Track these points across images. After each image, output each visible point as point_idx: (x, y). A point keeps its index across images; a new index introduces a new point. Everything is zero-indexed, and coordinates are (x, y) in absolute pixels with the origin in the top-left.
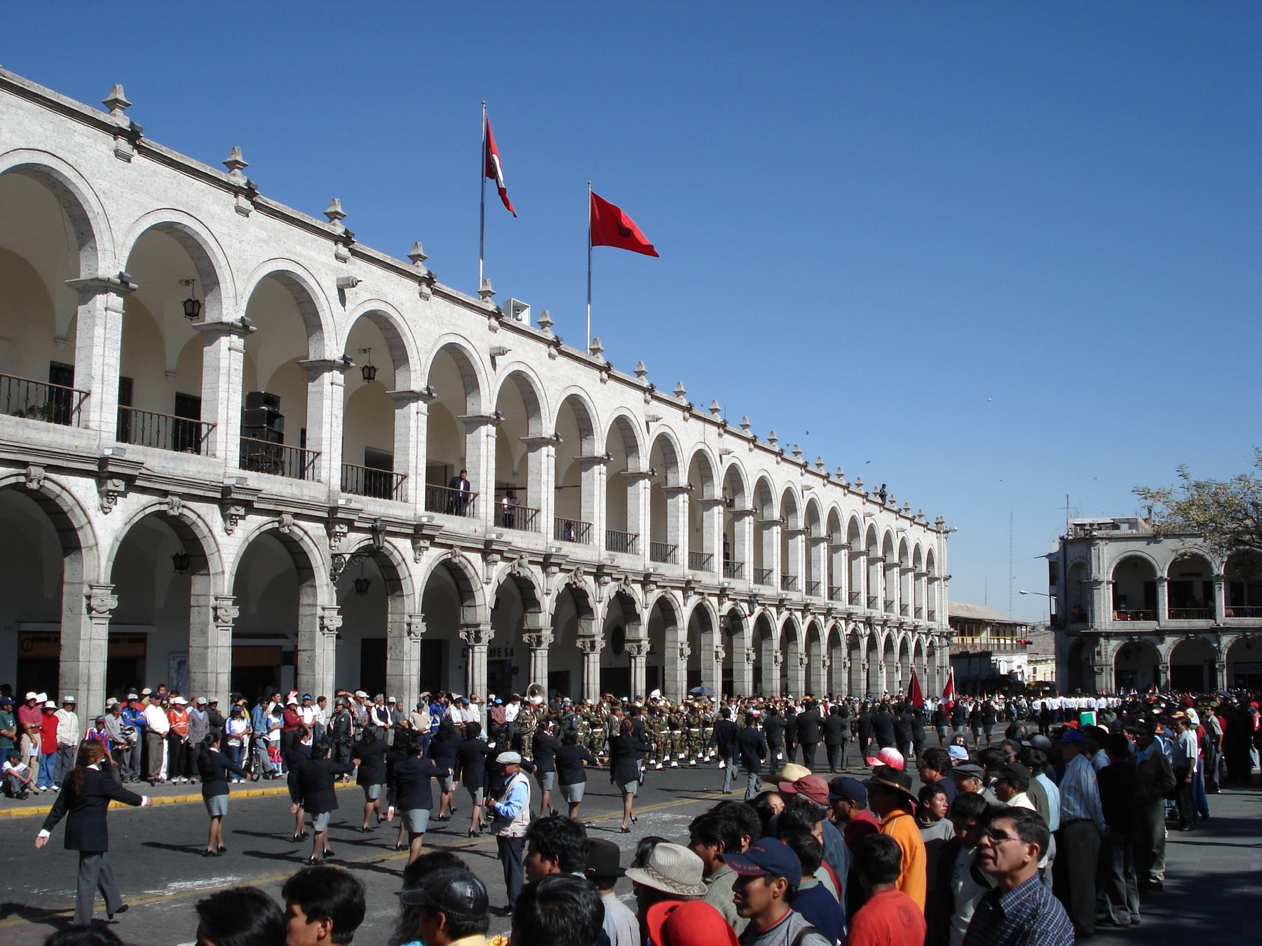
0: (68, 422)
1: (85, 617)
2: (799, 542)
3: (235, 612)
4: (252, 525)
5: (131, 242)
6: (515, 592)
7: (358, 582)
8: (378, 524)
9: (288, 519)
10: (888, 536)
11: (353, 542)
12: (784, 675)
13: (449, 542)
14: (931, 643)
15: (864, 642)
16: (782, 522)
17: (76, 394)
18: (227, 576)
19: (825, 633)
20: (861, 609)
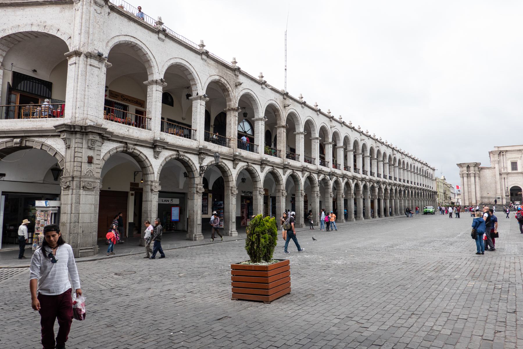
1: (150, 193)
5: (164, 71)
6: (271, 177)
9: (131, 146)
10: (399, 160)
11: (208, 161)
12: (355, 203)
13: (177, 149)
16: (383, 161)
19: (362, 187)
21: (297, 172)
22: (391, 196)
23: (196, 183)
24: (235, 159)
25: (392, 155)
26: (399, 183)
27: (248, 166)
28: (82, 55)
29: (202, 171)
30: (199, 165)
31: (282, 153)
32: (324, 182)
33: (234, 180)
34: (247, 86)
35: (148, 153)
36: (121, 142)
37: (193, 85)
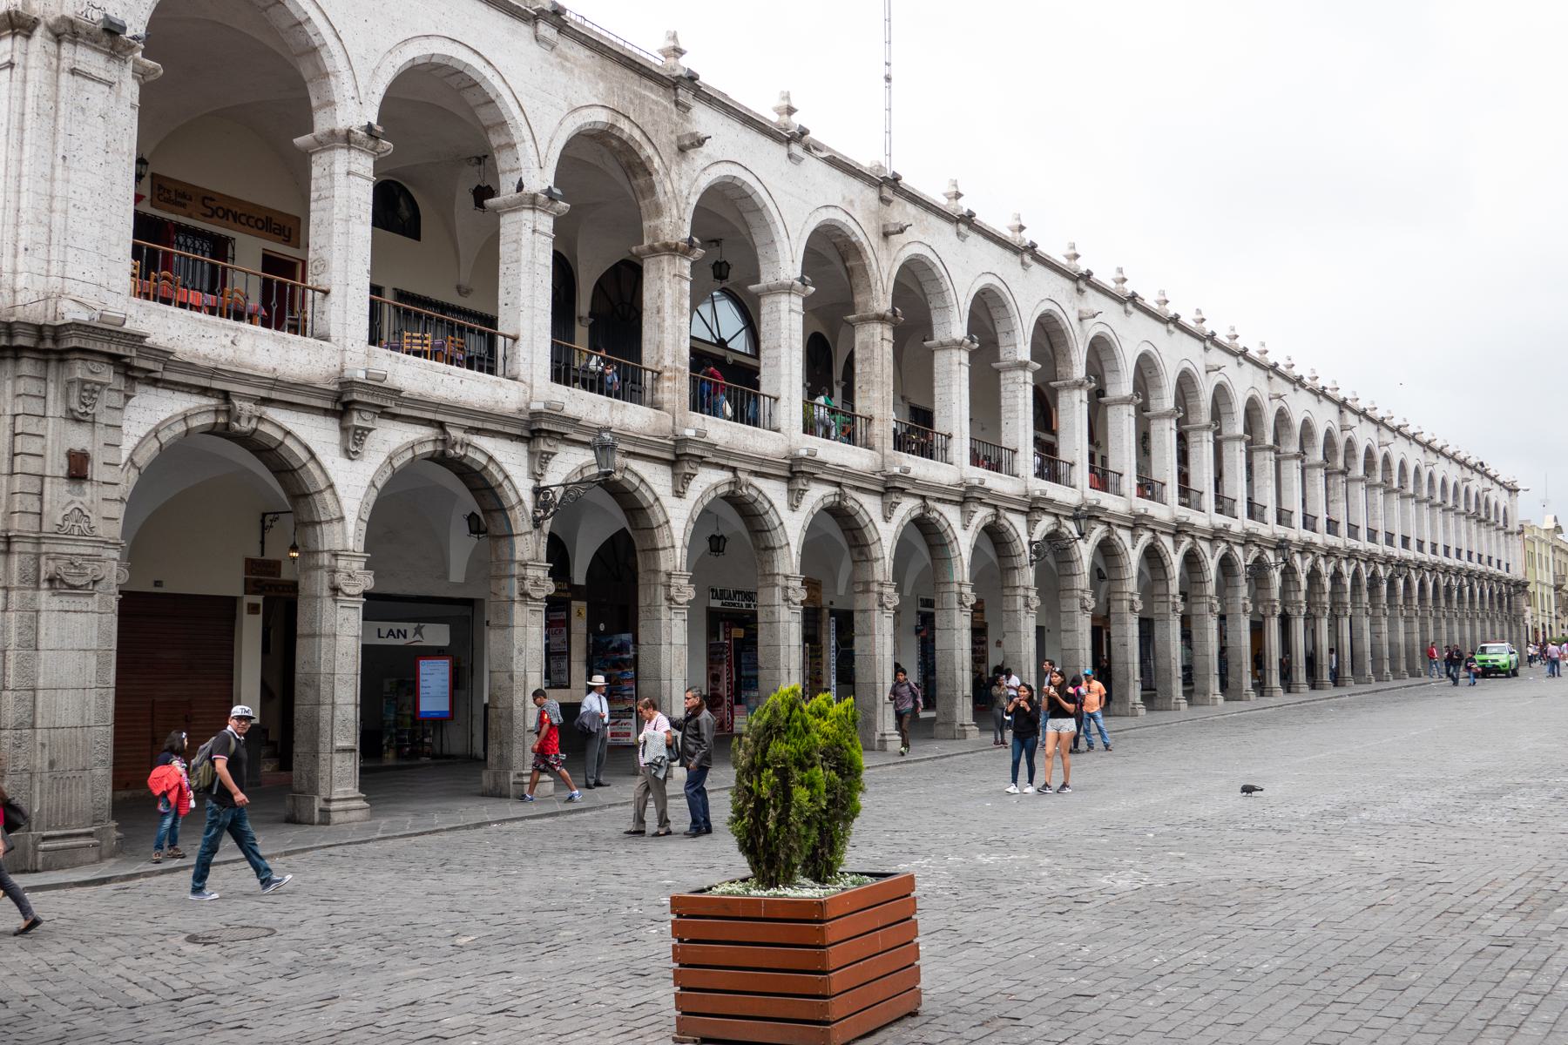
0: (805, 432)
2: (1319, 475)
3: (803, 595)
4: (392, 440)
5: (381, 90)
6: (733, 523)
7: (713, 539)
8: (607, 436)
10: (1369, 453)
11: (568, 464)
13: (440, 418)
14: (1374, 574)
15: (1276, 577)
17: (500, 339)
18: (678, 551)
20: (1269, 529)
21: (939, 506)
22: (1336, 603)
23: (518, 556)
24: (681, 458)
25: (1337, 432)
26: (1370, 546)
27: (736, 483)
28: (39, 32)
29: (545, 506)
30: (531, 483)
31: (876, 428)
32: (1055, 550)
33: (679, 543)
34: (728, 151)
35: (314, 434)
36: (204, 391)
37: (501, 147)
